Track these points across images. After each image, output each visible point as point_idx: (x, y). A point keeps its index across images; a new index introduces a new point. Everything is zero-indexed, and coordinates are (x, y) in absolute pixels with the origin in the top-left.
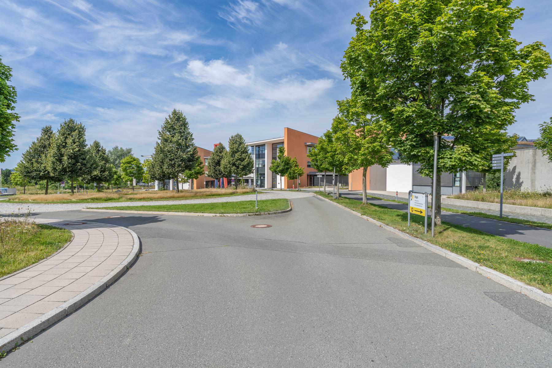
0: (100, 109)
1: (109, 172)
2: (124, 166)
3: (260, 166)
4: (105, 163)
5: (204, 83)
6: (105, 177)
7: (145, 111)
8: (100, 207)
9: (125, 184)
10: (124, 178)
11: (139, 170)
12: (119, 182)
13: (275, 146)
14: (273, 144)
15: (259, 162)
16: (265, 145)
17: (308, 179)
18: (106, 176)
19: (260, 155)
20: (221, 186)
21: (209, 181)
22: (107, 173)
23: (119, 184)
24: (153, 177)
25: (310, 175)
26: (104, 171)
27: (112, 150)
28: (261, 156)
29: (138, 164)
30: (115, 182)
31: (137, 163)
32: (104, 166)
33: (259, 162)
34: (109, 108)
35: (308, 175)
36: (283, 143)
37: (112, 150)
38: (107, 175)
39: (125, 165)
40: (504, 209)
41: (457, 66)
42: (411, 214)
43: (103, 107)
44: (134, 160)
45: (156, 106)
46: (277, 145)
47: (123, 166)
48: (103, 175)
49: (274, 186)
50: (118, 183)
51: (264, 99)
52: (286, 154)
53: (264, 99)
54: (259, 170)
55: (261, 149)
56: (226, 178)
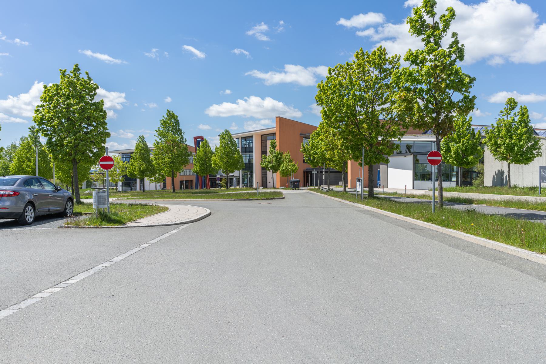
8: (4, 210)
13: (264, 138)
14: (262, 135)
15: (246, 157)
16: (252, 136)
17: (304, 176)
19: (247, 148)
20: (306, 185)
21: (189, 180)
25: (307, 172)
28: (247, 150)
33: (246, 157)
35: (304, 172)
36: (274, 134)
40: (384, 191)
41: (424, 122)
42: (342, 181)
46: (267, 136)
49: (264, 184)
52: (278, 148)
55: (248, 141)
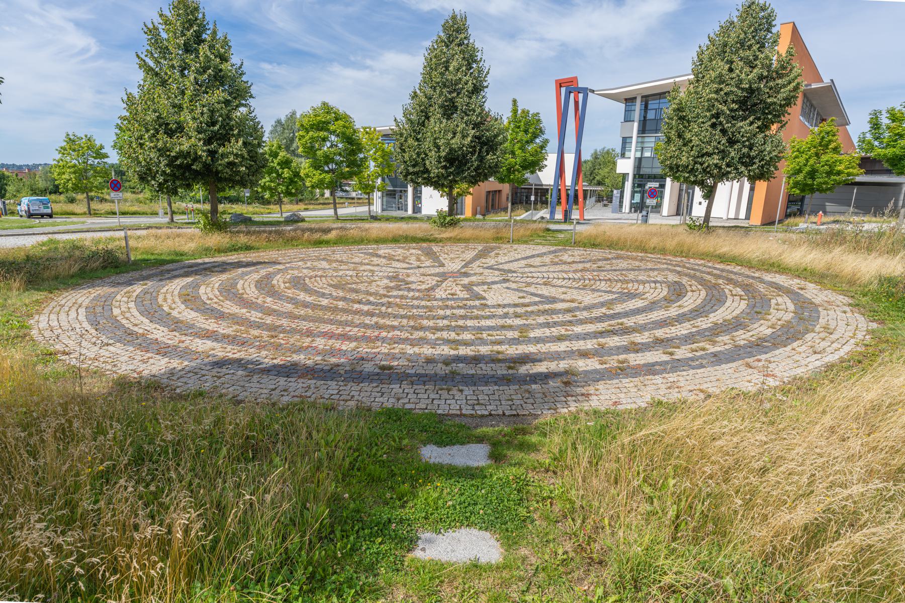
0: (266, 66)
1: (245, 143)
2: (307, 138)
3: (647, 154)
4: (227, 103)
5: (434, 10)
6: (231, 164)
7: (336, 68)
9: (311, 192)
10: (307, 176)
11: (353, 153)
12: (296, 190)
16: (635, 98)
18: (231, 158)
22: (236, 146)
23: (243, 202)
24: (411, 169)
26: (223, 138)
27: (283, 120)
29: (349, 132)
30: (287, 188)
31: (344, 127)
32: (224, 112)
34: (279, 64)
37: (283, 120)
38: (236, 155)
39: (311, 133)
43: (270, 62)
44: (337, 119)
45: (352, 59)
47: (303, 137)
48: (223, 156)
50: (293, 191)
51: (542, 40)
53: (542, 40)
54: (643, 164)
56: (677, 184)
